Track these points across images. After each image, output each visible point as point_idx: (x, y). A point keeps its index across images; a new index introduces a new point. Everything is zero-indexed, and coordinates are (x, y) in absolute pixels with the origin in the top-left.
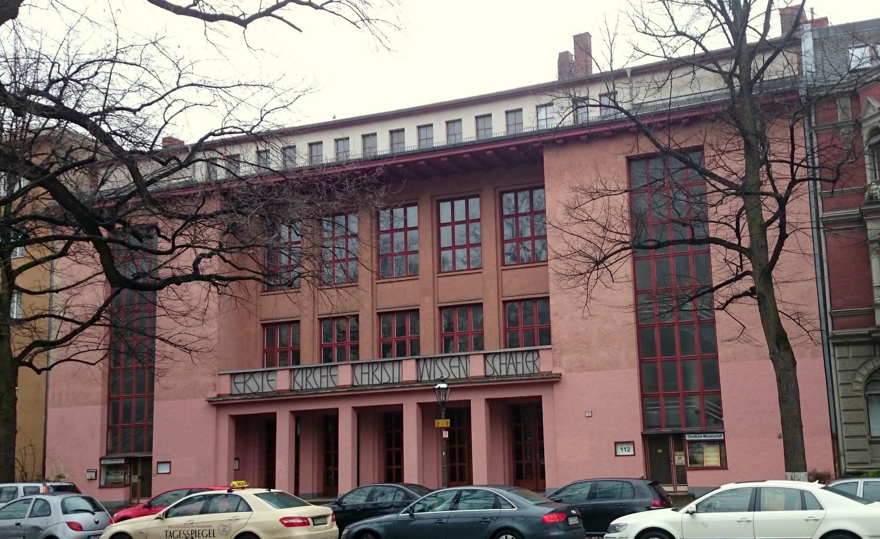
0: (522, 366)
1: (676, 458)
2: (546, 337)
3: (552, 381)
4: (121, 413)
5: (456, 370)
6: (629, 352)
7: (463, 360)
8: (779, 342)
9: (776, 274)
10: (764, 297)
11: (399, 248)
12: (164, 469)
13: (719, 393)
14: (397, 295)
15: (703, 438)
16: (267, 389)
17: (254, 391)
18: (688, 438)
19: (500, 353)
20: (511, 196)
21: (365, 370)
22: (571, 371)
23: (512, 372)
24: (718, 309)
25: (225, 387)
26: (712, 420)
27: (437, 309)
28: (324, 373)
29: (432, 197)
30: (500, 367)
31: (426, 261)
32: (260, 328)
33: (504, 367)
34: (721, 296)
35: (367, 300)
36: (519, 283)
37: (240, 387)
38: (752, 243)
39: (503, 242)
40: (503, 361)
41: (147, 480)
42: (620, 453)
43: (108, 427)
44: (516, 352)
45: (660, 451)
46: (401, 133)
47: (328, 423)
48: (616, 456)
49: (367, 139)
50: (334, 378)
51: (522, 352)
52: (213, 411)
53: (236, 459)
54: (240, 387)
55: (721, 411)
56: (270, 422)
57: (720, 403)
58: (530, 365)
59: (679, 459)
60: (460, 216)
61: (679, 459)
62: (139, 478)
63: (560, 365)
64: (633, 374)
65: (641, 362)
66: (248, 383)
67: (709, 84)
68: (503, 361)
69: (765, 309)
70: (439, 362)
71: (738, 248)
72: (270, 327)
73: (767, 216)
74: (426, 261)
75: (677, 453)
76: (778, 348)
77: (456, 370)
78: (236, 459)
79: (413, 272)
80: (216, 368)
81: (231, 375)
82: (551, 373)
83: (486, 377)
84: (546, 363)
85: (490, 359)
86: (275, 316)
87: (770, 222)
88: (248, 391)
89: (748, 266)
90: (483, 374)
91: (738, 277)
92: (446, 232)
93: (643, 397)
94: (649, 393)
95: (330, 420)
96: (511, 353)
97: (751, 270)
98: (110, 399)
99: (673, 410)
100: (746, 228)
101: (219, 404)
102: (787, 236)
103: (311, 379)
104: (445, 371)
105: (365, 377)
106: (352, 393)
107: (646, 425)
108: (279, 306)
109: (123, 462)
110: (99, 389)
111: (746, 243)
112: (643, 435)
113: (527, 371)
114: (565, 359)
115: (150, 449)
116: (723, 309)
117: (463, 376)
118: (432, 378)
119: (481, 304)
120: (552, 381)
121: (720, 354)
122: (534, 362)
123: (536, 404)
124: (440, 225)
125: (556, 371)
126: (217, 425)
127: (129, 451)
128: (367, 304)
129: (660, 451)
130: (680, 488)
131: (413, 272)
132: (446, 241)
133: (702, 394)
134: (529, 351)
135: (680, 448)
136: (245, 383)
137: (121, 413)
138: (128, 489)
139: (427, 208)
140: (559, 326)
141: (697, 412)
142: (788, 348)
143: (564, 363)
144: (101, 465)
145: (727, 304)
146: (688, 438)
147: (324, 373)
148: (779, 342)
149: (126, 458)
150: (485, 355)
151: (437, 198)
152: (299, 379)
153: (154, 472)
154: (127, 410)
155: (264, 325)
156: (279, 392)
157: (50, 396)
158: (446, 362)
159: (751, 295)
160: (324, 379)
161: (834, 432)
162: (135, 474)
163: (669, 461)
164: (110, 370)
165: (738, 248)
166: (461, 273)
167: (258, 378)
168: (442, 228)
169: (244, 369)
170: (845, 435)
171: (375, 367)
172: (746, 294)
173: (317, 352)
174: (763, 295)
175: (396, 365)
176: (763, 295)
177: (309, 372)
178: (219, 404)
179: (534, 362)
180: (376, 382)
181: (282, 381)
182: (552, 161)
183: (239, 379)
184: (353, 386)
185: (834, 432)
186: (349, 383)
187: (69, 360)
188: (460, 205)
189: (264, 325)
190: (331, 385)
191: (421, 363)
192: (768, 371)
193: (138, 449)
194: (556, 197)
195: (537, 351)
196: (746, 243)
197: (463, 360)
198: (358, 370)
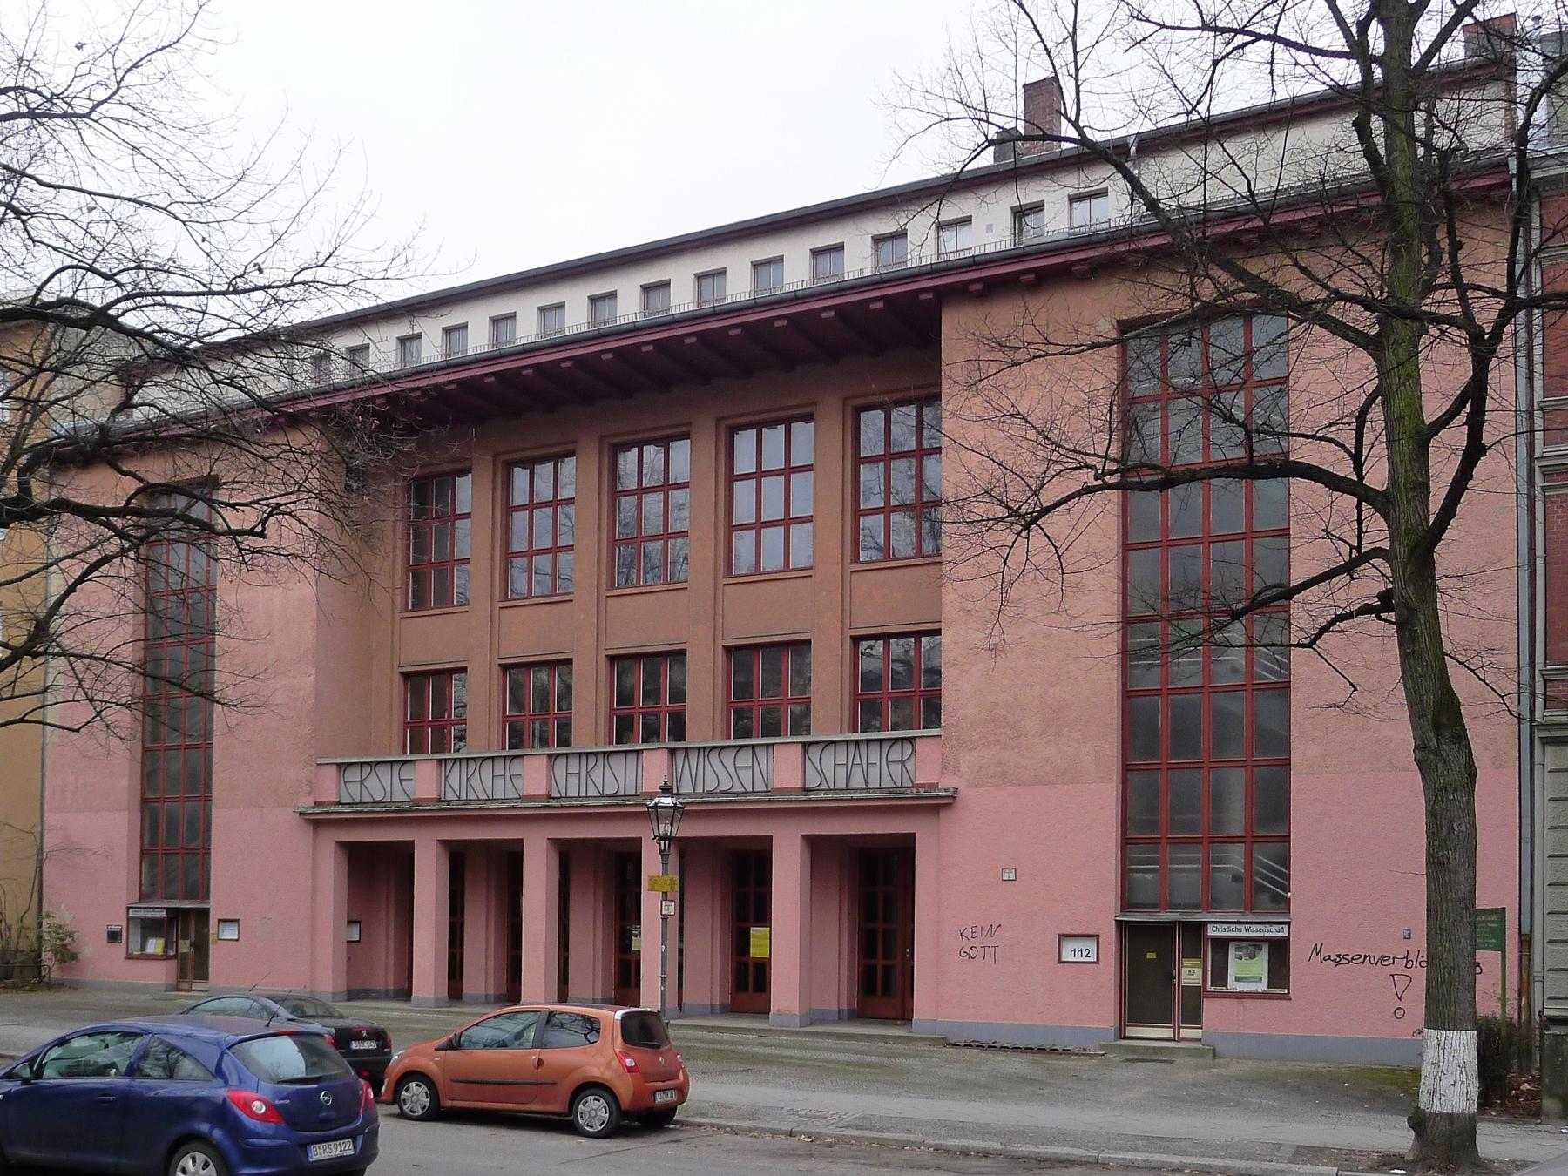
0: (876, 770)
1: (1184, 971)
2: (932, 712)
3: (937, 805)
4: (163, 827)
5: (745, 775)
6: (1100, 746)
7: (761, 754)
8: (1440, 725)
9: (1448, 556)
10: (1413, 611)
11: (653, 525)
12: (230, 933)
13: (1286, 839)
14: (643, 623)
15: (1244, 933)
16: (399, 796)
17: (378, 798)
18: (1212, 931)
19: (835, 743)
20: (878, 416)
21: (574, 766)
22: (979, 785)
23: (857, 782)
24: (1298, 645)
25: (329, 788)
26: (1265, 897)
27: (720, 651)
28: (499, 770)
29: (719, 420)
30: (834, 772)
31: (699, 554)
32: (397, 678)
33: (842, 772)
34: (1305, 612)
35: (584, 627)
36: (883, 601)
37: (355, 789)
38: (1393, 480)
39: (858, 513)
40: (841, 759)
41: (201, 947)
42: (1067, 955)
43: (143, 853)
44: (868, 741)
45: (1151, 956)
46: (662, 292)
47: (619, 868)
48: (1060, 962)
49: (600, 304)
50: (517, 782)
51: (880, 741)
52: (309, 830)
53: (350, 922)
54: (355, 789)
55: (1287, 877)
56: (403, 855)
57: (1285, 861)
58: (896, 770)
59: (1191, 974)
60: (773, 460)
61: (1191, 974)
62: (192, 945)
63: (956, 772)
64: (1107, 795)
65: (1126, 769)
66: (367, 783)
67: (1328, 151)
68: (841, 759)
69: (1413, 640)
70: (714, 754)
71: (1357, 489)
72: (415, 679)
73: (1432, 410)
74: (699, 554)
75: (1187, 962)
76: (1438, 736)
77: (745, 775)
78: (350, 922)
79: (669, 579)
80: (312, 752)
81: (339, 765)
82: (935, 786)
83: (806, 790)
84: (926, 765)
85: (814, 753)
86: (423, 659)
87: (1443, 423)
88: (367, 799)
89: (1378, 532)
90: (799, 785)
91: (1349, 568)
92: (744, 493)
93: (1126, 842)
94: (1139, 835)
95: (509, 860)
96: (857, 742)
97: (1386, 545)
98: (144, 802)
99: (1186, 869)
100: (1381, 449)
101: (318, 822)
102: (1482, 451)
103: (475, 781)
104: (727, 773)
105: (573, 780)
106: (547, 812)
107: (1127, 904)
108: (430, 640)
109: (163, 915)
110: (124, 783)
111: (1377, 476)
112: (1119, 924)
113: (887, 783)
114: (967, 759)
115: (206, 896)
116: (1309, 646)
117: (760, 787)
118: (699, 790)
119: (808, 642)
120: (937, 805)
121: (1295, 758)
122: (903, 763)
123: (901, 853)
124: (732, 478)
125: (947, 783)
126: (314, 855)
127: (171, 897)
128: (589, 640)
129: (1151, 956)
130: (1187, 1033)
131: (669, 579)
132: (744, 511)
133: (1249, 840)
134: (895, 740)
135: (1193, 952)
136: (361, 782)
137: (163, 827)
138: (173, 963)
139: (708, 447)
140: (957, 692)
141: (1236, 878)
142: (1461, 738)
143: (964, 768)
144: (129, 919)
145: (1318, 636)
146: (1212, 931)
147: (499, 770)
148: (1440, 725)
149: (168, 909)
150: (806, 746)
151: (729, 422)
152: (454, 779)
153: (211, 938)
154: (172, 824)
155: (406, 676)
156: (416, 802)
157: (47, 794)
158: (728, 757)
159: (1376, 611)
160: (499, 783)
161: (1526, 930)
162: (185, 937)
163: (1169, 976)
164: (145, 750)
165: (1357, 489)
166: (773, 578)
167: (384, 773)
168: (737, 485)
169: (367, 756)
170: (1547, 938)
171: (592, 760)
172: (1366, 610)
173: (496, 728)
174: (1411, 607)
175: (632, 758)
176: (1411, 607)
177: (472, 765)
178: (318, 822)
179: (903, 763)
180: (593, 792)
181: (423, 781)
182: (960, 334)
183: (353, 775)
184: (550, 797)
185: (1526, 930)
186: (543, 792)
187: (22, 720)
188: (774, 437)
189: (406, 676)
190: (511, 794)
191: (680, 757)
192: (1408, 795)
193: (190, 895)
194: (962, 416)
195: (911, 740)
196: (1377, 476)
197: (761, 754)
198: (560, 765)
